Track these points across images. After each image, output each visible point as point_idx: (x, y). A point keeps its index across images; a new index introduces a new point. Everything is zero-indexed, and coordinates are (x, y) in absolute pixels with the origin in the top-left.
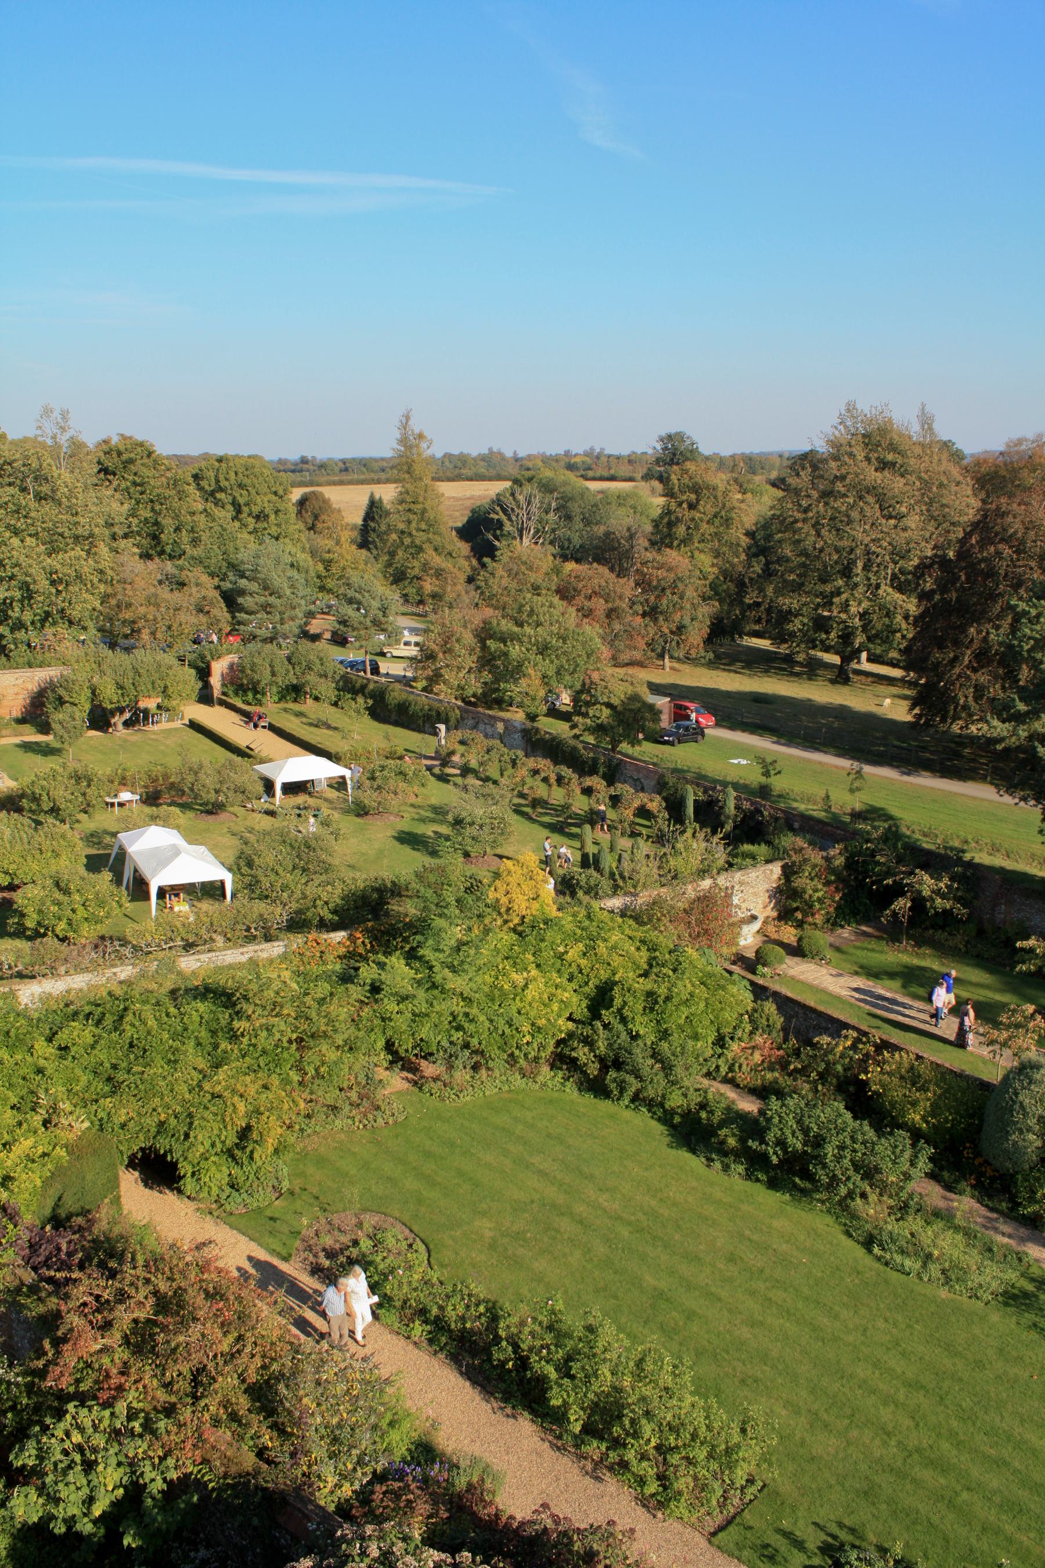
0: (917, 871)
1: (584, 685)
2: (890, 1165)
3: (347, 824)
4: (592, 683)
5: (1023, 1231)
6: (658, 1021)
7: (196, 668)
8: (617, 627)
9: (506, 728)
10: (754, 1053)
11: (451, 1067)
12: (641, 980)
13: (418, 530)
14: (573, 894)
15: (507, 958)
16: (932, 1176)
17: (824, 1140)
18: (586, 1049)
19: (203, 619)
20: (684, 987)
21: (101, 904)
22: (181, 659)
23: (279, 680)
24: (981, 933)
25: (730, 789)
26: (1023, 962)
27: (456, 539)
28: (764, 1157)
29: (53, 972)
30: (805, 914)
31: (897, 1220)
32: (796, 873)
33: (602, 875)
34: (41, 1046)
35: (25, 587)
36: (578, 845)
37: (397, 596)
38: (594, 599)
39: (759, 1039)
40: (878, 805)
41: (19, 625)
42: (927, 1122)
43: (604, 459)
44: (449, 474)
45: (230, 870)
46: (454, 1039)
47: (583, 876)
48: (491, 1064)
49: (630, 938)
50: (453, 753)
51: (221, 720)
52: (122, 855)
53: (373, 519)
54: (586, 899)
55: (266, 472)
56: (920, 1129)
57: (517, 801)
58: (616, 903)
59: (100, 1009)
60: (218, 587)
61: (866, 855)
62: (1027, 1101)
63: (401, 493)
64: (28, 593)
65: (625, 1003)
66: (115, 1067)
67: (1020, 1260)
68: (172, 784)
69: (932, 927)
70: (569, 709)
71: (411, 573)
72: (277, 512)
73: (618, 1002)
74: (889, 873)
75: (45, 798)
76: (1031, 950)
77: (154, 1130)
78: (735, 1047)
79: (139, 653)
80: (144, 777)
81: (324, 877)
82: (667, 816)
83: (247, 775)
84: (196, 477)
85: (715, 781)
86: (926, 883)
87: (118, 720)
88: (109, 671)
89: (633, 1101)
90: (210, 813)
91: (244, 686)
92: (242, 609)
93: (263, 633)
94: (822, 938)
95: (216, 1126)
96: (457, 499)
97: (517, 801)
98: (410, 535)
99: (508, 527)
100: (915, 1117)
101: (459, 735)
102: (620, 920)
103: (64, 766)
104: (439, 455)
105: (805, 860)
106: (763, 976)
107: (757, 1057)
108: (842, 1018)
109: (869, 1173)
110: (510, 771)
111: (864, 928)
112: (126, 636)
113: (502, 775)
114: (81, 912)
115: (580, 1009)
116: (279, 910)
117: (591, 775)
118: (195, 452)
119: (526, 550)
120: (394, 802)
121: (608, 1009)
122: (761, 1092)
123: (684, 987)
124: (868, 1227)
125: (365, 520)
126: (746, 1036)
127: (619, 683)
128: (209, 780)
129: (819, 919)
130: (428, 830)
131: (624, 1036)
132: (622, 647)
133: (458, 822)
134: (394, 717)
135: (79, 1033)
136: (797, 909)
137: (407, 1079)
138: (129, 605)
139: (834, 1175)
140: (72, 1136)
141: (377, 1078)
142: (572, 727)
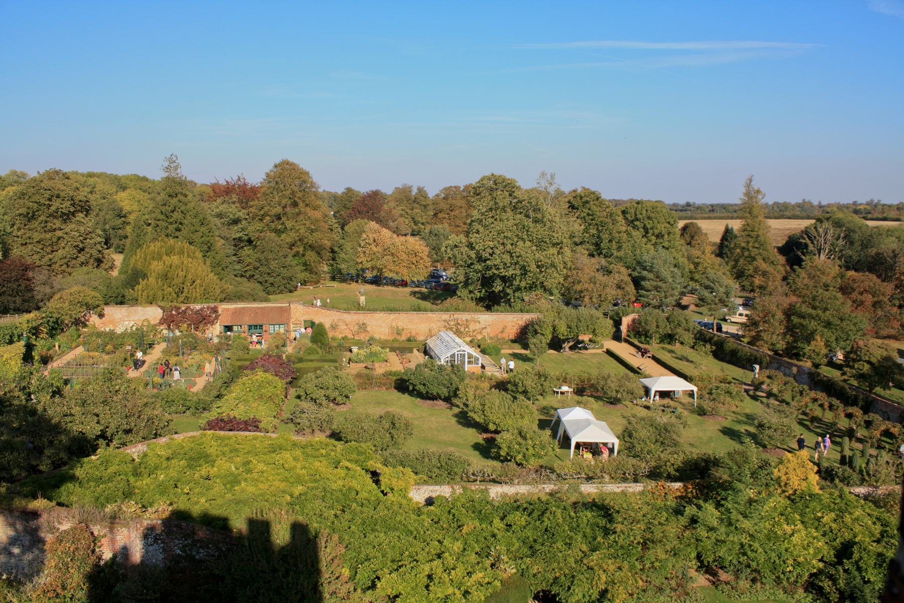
1: (853, 348)
3: (692, 419)
4: (858, 347)
7: (614, 320)
8: (880, 313)
9: (798, 371)
11: (737, 578)
12: (875, 544)
13: (754, 247)
14: (832, 480)
15: (782, 515)
18: (830, 583)
19: (620, 292)
21: (543, 447)
22: (605, 314)
23: (661, 331)
27: (777, 254)
29: (510, 482)
33: (854, 471)
34: (497, 522)
35: (523, 268)
36: (839, 449)
37: (737, 286)
38: (865, 295)
41: (518, 289)
43: (880, 207)
44: (776, 214)
45: (618, 437)
46: (741, 560)
47: (840, 470)
48: (764, 580)
49: (869, 515)
50: (762, 383)
51: (623, 350)
52: (559, 421)
53: (726, 240)
54: (840, 485)
55: (664, 210)
57: (801, 417)
58: (862, 490)
59: (532, 507)
60: (630, 275)
63: (744, 225)
64: (524, 271)
65: (861, 558)
66: (535, 541)
68: (592, 385)
70: (841, 362)
71: (747, 273)
72: (669, 233)
73: (856, 556)
75: (520, 385)
77: (551, 581)
79: (582, 309)
80: (577, 379)
81: (672, 449)
83: (635, 383)
84: (624, 212)
87: (566, 346)
88: (564, 318)
90: (612, 403)
91: (640, 333)
92: (643, 288)
93: (654, 302)
95: (587, 586)
96: (780, 229)
97: (801, 417)
98: (748, 250)
99: (811, 247)
101: (767, 372)
102: (862, 502)
103: (533, 368)
104: (771, 203)
110: (798, 398)
112: (576, 299)
113: (793, 400)
114: (531, 451)
115: (830, 555)
116: (643, 465)
117: (852, 405)
118: (625, 198)
119: (823, 263)
120: (722, 409)
121: (848, 559)
125: (722, 240)
127: (877, 349)
128: (613, 385)
130: (742, 428)
131: (858, 579)
132: (882, 326)
133: (761, 426)
134: (728, 358)
135: (519, 519)
137: (708, 579)
138: (579, 282)
140: (505, 576)
141: (689, 575)
142: (843, 374)
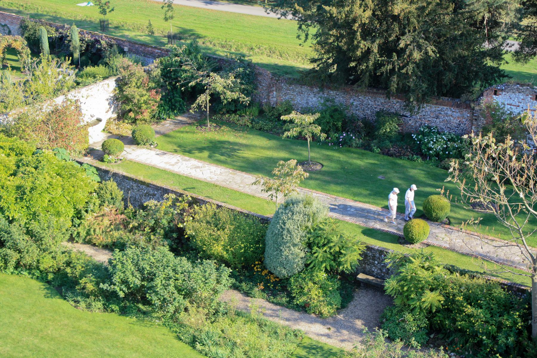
0: (211, 74)
2: (202, 285)
5: (296, 314)
6: (28, 207)
10: (103, 220)
12: (11, 178)
16: (235, 287)
17: (155, 275)
20: (43, 180)
24: (261, 112)
25: (74, 27)
26: (289, 130)
28: (114, 294)
30: (137, 113)
31: (212, 323)
32: (126, 84)
39: (106, 209)
40: (188, 28)
42: (227, 251)
56: (222, 257)
61: (175, 66)
62: (292, 227)
67: (296, 335)
69: (228, 112)
74: (192, 78)
76: (291, 121)
78: (89, 217)
82: (29, 51)
85: (65, 21)
86: (218, 82)
89: (16, 268)
94: (149, 129)
100: (218, 249)
105: (131, 75)
106: (109, 162)
107: (106, 222)
108: (164, 186)
109: (188, 294)
111: (180, 118)
122: (109, 247)
123: (43, 180)
124: (191, 331)
126: (97, 208)
129: (147, 115)
136: (130, 110)
139: (164, 299)
